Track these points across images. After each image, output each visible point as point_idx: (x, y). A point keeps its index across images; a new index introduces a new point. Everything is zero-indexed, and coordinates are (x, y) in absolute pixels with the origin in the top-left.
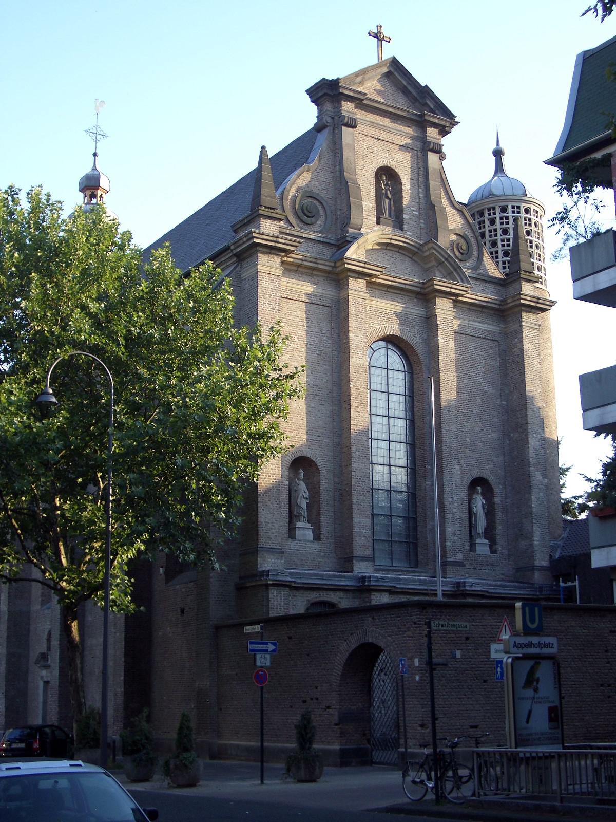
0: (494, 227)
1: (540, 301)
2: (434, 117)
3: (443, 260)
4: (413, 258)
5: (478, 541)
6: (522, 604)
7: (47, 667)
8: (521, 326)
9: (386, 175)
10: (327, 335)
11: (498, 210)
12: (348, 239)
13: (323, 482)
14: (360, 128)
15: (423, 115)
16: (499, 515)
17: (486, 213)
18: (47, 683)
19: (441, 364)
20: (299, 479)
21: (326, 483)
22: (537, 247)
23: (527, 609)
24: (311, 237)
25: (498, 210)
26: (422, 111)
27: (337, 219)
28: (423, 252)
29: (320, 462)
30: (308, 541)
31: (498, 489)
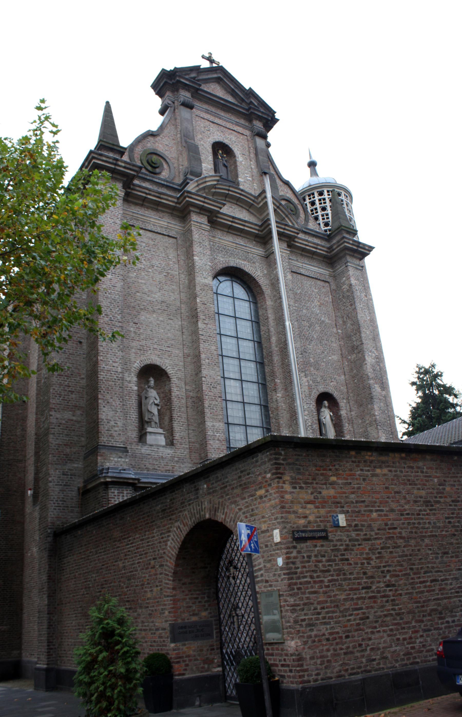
0: (315, 207)
4: (250, 210)
10: (174, 260)
11: (316, 194)
21: (179, 389)
25: (316, 194)
28: (258, 204)
30: (160, 446)
31: (342, 404)
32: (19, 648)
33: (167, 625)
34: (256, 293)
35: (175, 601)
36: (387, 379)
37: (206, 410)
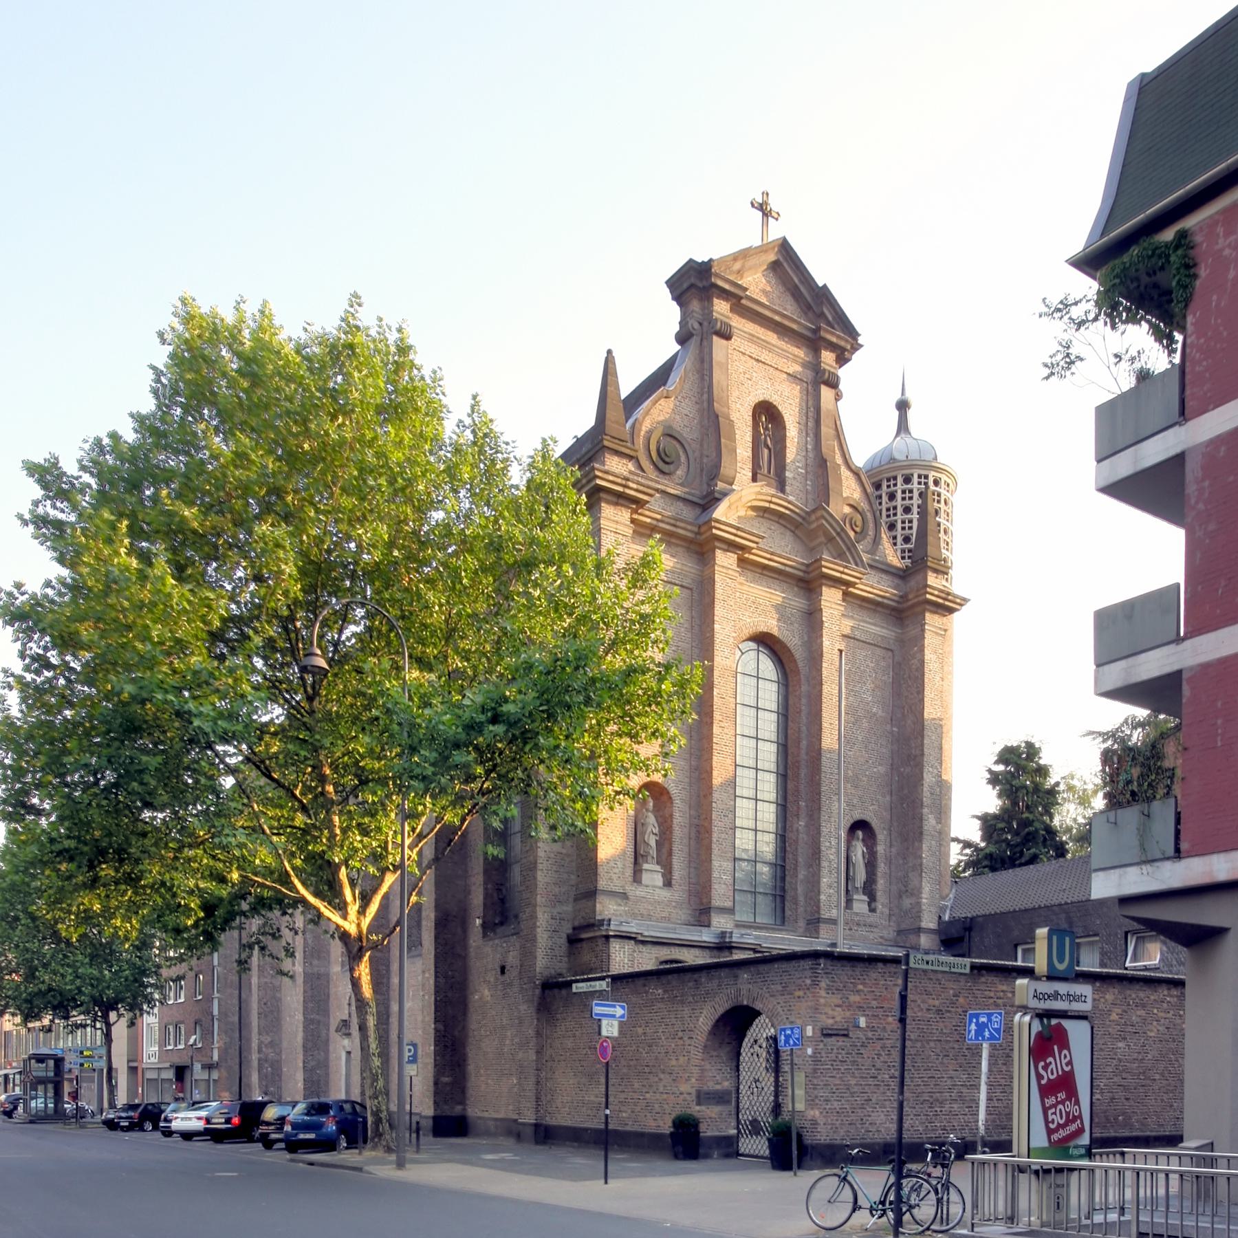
0: (894, 503)
2: (833, 334)
5: (855, 897)
7: (349, 1035)
8: (923, 630)
9: (766, 413)
11: (900, 480)
12: (717, 495)
13: (677, 815)
15: (818, 329)
16: (882, 868)
17: (885, 484)
18: (349, 1053)
22: (945, 532)
23: (1055, 938)
24: (672, 491)
25: (900, 480)
26: (819, 326)
27: (702, 470)
28: (809, 523)
29: (673, 790)
31: (881, 836)
32: (462, 1102)
33: (693, 1091)
36: (950, 799)
37: (714, 846)
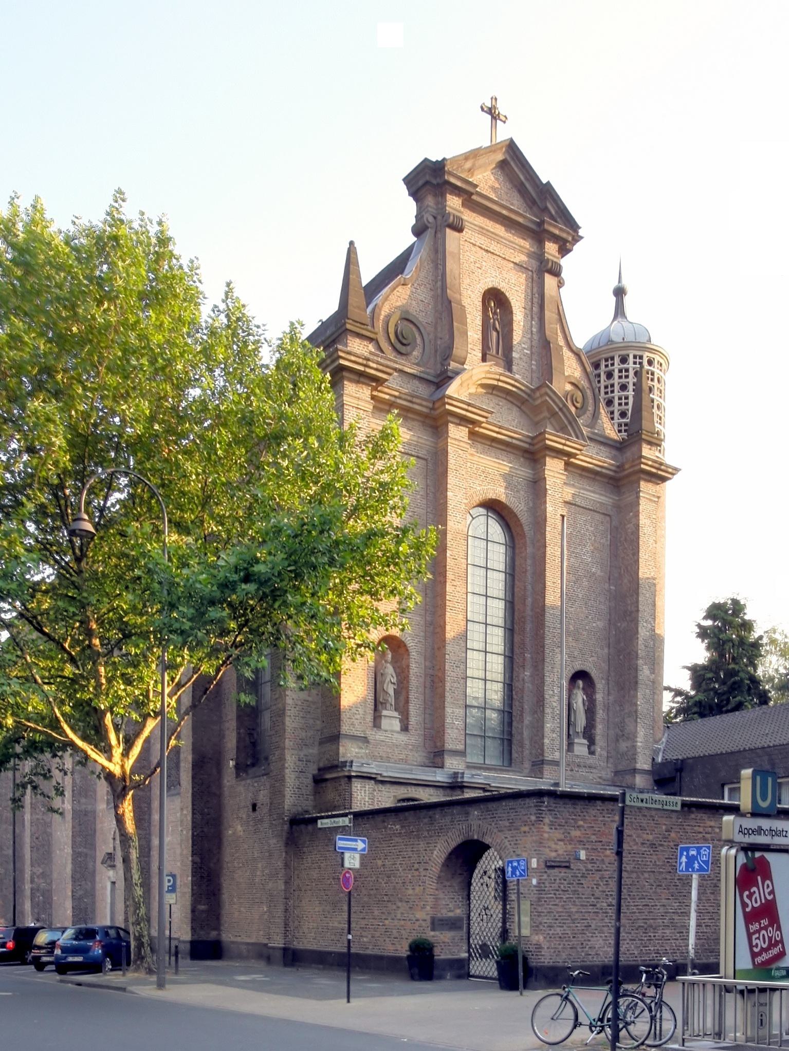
0: (611, 381)
1: (663, 467)
3: (557, 410)
6: (753, 771)
7: (113, 866)
8: (638, 497)
9: (495, 299)
11: (617, 360)
12: (450, 374)
14: (467, 233)
16: (600, 714)
17: (603, 364)
18: (114, 883)
19: (548, 536)
20: (386, 661)
23: (758, 778)
24: (409, 370)
25: (617, 360)
27: (436, 351)
28: (535, 400)
29: (410, 643)
34: (515, 534)
35: (437, 899)
37: (447, 694)
